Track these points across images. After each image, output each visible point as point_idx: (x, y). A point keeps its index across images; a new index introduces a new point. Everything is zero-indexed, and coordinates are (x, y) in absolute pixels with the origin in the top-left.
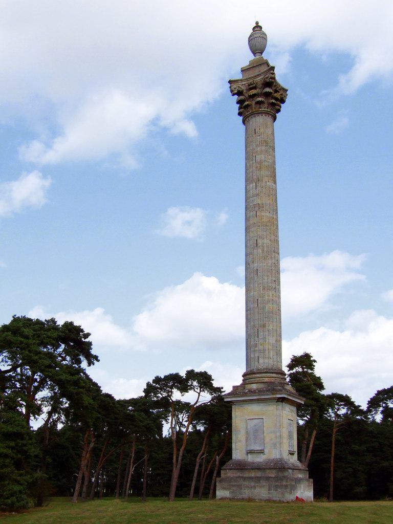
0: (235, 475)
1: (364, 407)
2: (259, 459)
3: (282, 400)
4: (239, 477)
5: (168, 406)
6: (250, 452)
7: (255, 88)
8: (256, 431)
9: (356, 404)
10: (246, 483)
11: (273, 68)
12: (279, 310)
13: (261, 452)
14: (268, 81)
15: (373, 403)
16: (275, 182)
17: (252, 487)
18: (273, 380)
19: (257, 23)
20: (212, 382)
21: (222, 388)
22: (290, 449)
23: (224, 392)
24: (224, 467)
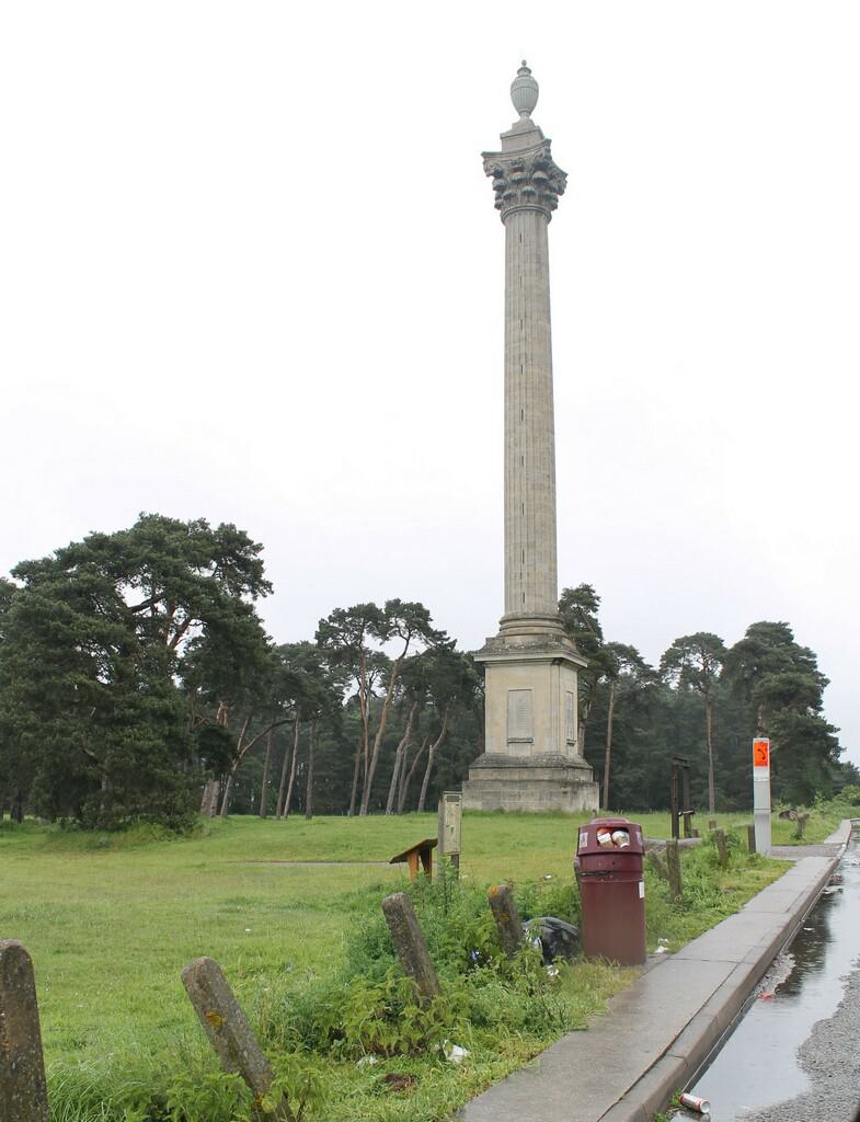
0: (491, 778)
1: (656, 668)
2: (524, 752)
3: (559, 662)
4: (496, 780)
5: (354, 658)
6: (512, 742)
7: (521, 169)
9: (645, 662)
10: (507, 789)
11: (548, 142)
12: (555, 522)
13: (530, 742)
15: (671, 658)
18: (545, 630)
19: (524, 63)
20: (260, 624)
21: (445, 633)
22: (569, 737)
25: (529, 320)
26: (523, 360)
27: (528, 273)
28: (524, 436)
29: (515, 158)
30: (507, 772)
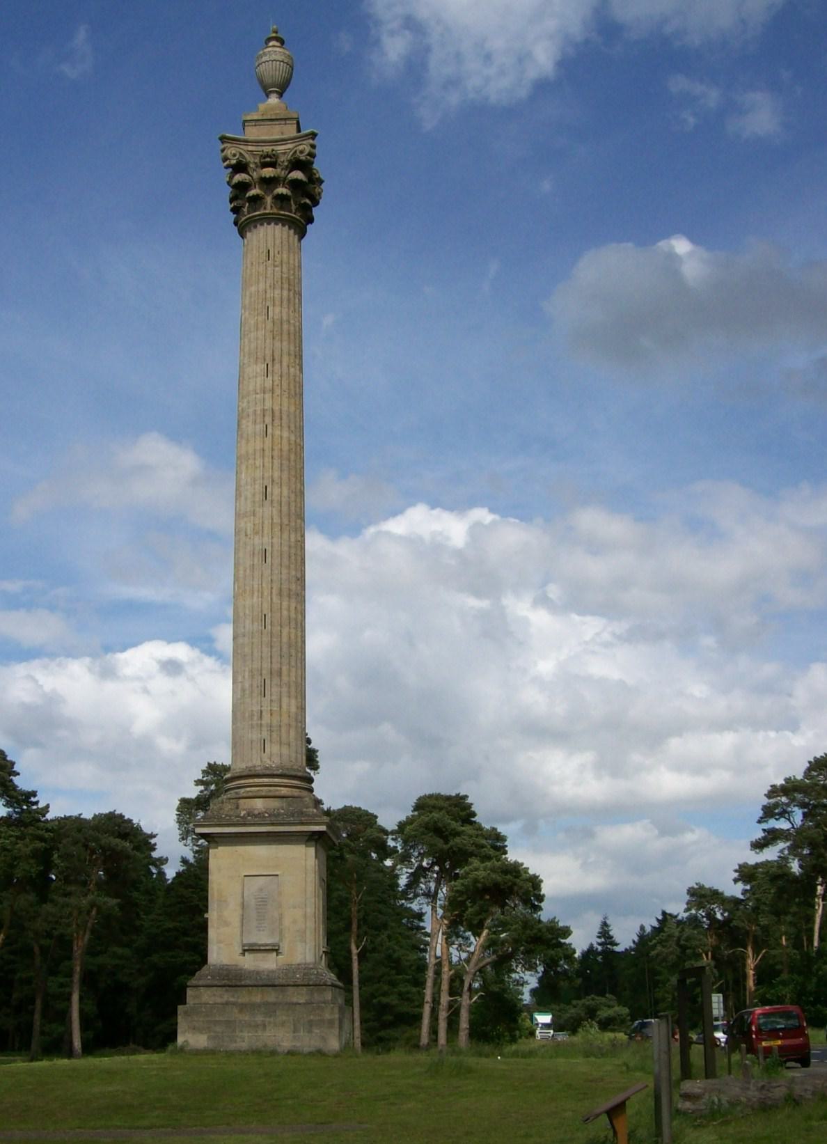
0: (219, 1000)
2: (268, 963)
4: (227, 1003)
6: (250, 949)
7: (273, 165)
8: (263, 902)
14: (303, 158)
16: (301, 370)
17: (257, 1026)
21: (34, 794)
23: (37, 803)
24: (193, 982)
25: (277, 366)
26: (268, 420)
27: (277, 303)
28: (267, 523)
29: (267, 149)
30: (244, 991)
